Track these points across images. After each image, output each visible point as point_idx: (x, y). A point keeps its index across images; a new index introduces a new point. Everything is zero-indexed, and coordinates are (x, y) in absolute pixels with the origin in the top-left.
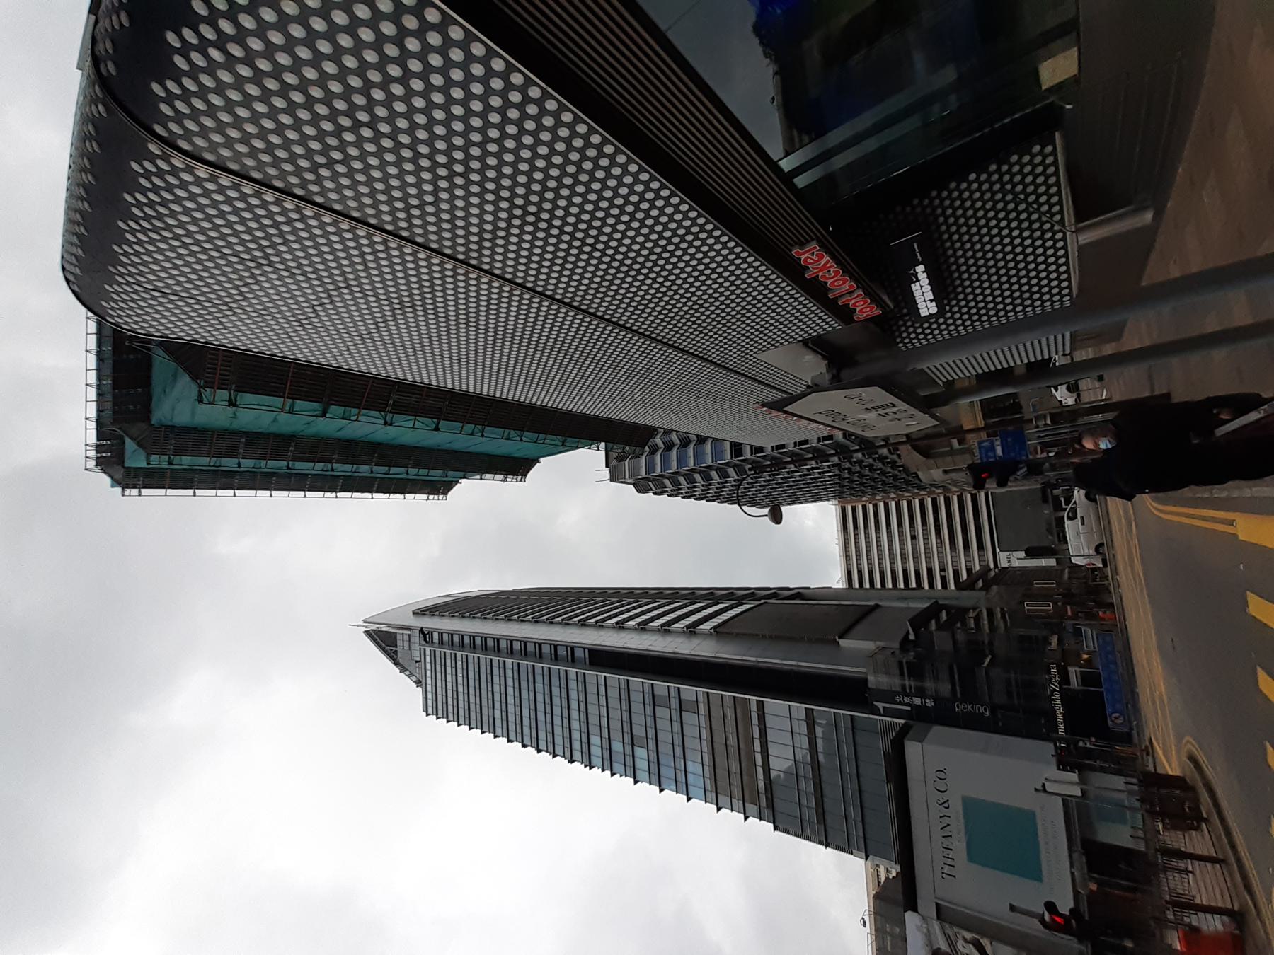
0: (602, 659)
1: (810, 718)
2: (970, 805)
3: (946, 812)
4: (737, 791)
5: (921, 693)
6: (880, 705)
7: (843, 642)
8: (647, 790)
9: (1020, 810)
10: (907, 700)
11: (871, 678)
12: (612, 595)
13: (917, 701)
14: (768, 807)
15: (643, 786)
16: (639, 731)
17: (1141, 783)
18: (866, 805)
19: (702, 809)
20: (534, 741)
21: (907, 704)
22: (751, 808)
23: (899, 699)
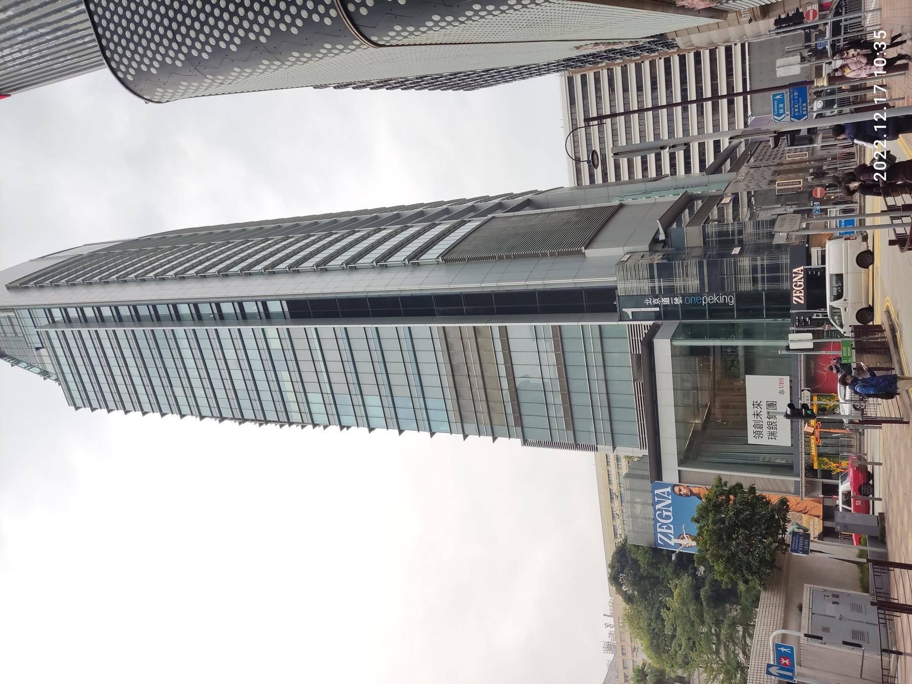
0: (304, 310)
4: (484, 417)
5: (670, 292)
6: (629, 311)
7: (589, 253)
8: (386, 436)
10: (656, 301)
12: (219, 236)
13: (666, 301)
14: (516, 425)
17: (675, 4)
19: (447, 442)
21: (656, 306)
23: (647, 301)
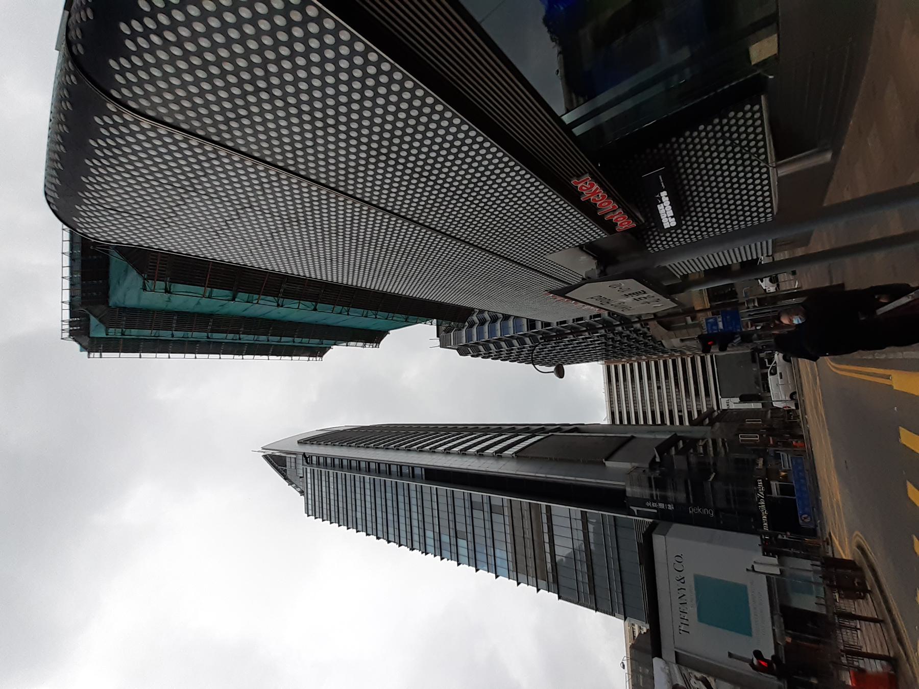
0: (434, 475)
1: (584, 518)
2: (700, 581)
3: (682, 586)
4: (531, 571)
5: (665, 500)
6: (635, 509)
7: (608, 463)
8: (467, 570)
9: (736, 584)
10: (654, 505)
11: (628, 489)
12: (442, 430)
13: (662, 506)
14: (554, 582)
15: (464, 567)
16: (461, 528)
18: (625, 581)
19: (506, 584)
20: (385, 534)
21: (654, 508)
22: (542, 583)
23: (648, 504)
